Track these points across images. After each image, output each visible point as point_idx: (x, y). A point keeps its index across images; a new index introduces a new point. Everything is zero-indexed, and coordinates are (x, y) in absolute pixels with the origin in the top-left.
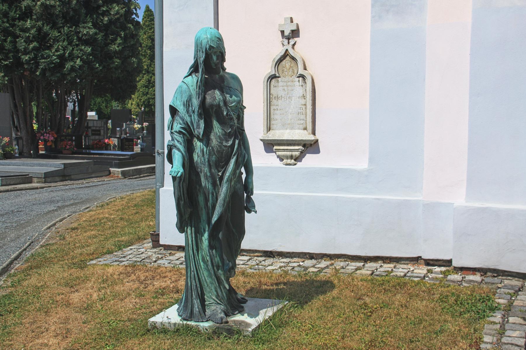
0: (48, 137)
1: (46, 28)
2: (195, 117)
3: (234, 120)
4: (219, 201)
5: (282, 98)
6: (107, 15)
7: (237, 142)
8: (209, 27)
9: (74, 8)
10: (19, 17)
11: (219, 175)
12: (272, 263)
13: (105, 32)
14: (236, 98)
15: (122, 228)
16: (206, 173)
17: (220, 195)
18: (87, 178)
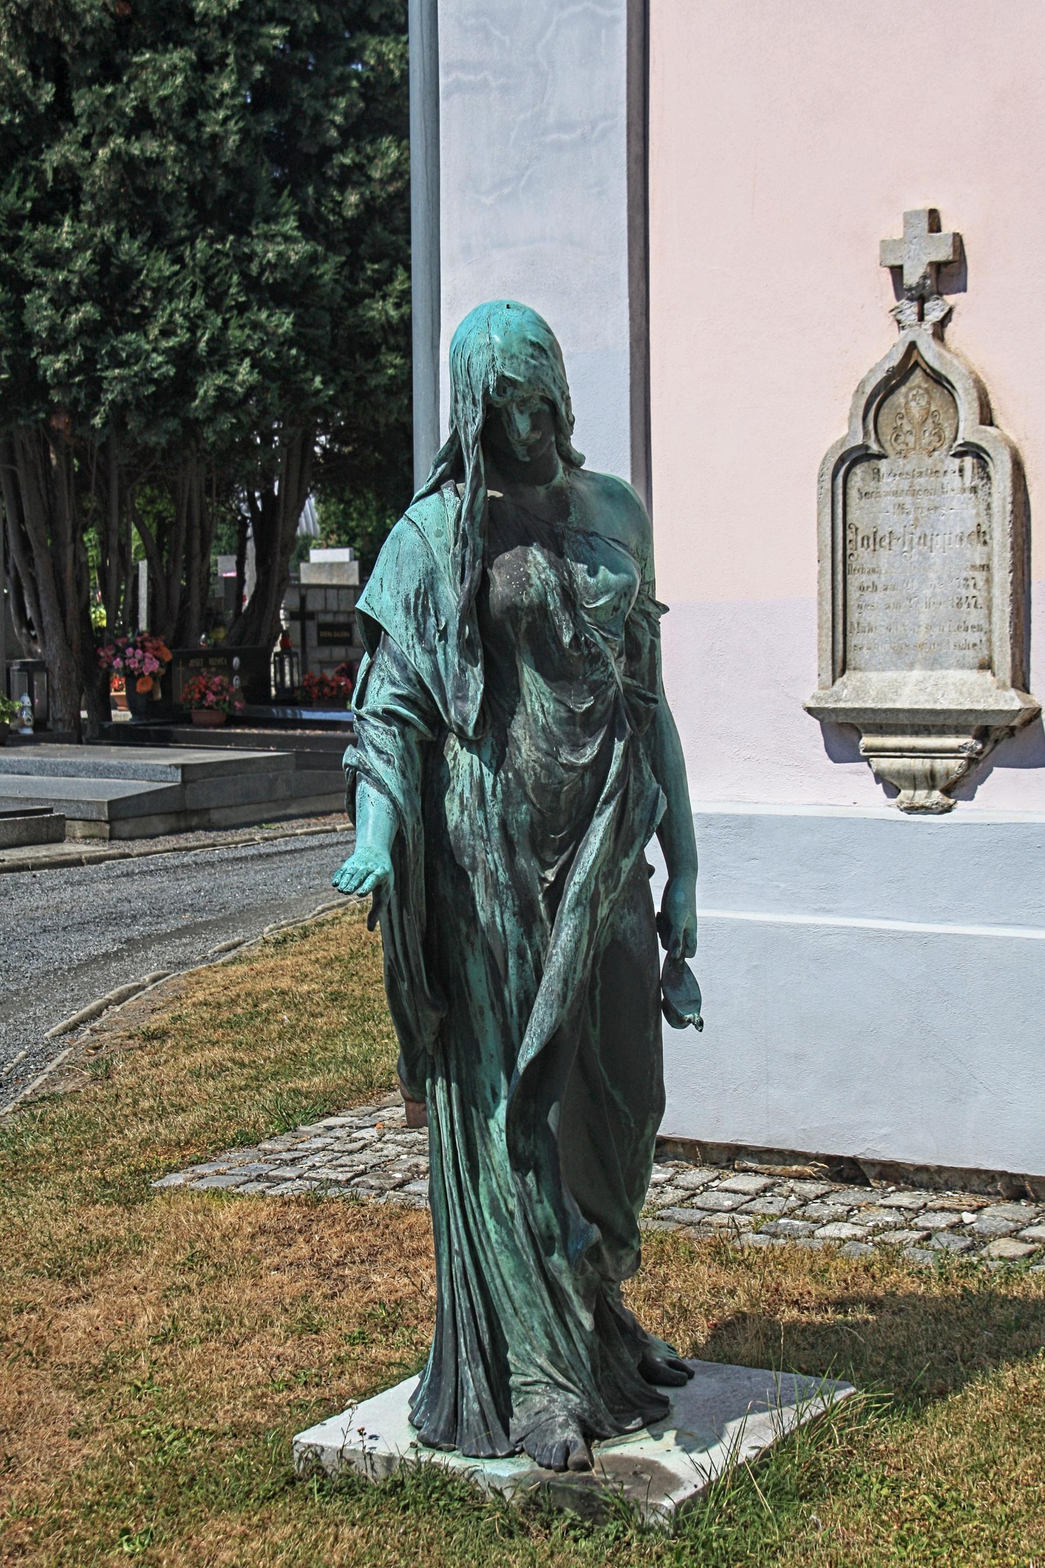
0: (140, 662)
1: (129, 248)
2: (450, 655)
3: (606, 665)
4: (545, 979)
5: (894, 542)
6: (357, 185)
7: (619, 747)
8: (501, 303)
9: (231, 165)
10: (33, 206)
11: (545, 880)
12: (852, 1210)
13: (348, 251)
14: (612, 577)
15: (328, 1035)
16: (494, 874)
17: (550, 960)
18: (268, 821)
